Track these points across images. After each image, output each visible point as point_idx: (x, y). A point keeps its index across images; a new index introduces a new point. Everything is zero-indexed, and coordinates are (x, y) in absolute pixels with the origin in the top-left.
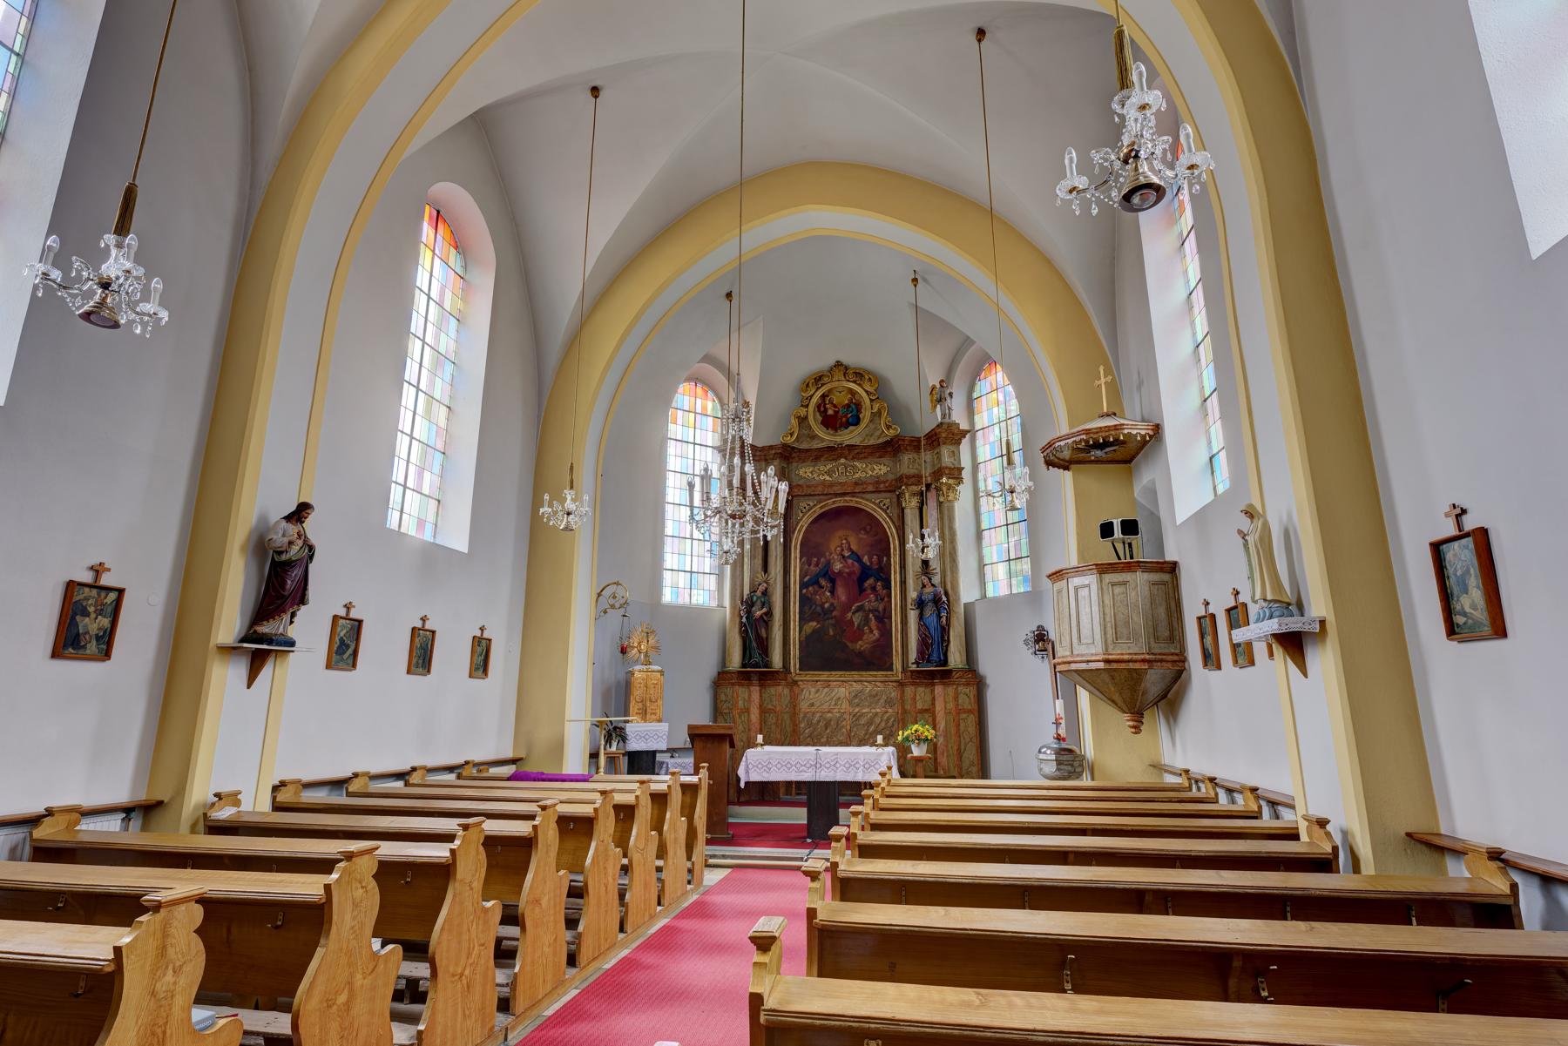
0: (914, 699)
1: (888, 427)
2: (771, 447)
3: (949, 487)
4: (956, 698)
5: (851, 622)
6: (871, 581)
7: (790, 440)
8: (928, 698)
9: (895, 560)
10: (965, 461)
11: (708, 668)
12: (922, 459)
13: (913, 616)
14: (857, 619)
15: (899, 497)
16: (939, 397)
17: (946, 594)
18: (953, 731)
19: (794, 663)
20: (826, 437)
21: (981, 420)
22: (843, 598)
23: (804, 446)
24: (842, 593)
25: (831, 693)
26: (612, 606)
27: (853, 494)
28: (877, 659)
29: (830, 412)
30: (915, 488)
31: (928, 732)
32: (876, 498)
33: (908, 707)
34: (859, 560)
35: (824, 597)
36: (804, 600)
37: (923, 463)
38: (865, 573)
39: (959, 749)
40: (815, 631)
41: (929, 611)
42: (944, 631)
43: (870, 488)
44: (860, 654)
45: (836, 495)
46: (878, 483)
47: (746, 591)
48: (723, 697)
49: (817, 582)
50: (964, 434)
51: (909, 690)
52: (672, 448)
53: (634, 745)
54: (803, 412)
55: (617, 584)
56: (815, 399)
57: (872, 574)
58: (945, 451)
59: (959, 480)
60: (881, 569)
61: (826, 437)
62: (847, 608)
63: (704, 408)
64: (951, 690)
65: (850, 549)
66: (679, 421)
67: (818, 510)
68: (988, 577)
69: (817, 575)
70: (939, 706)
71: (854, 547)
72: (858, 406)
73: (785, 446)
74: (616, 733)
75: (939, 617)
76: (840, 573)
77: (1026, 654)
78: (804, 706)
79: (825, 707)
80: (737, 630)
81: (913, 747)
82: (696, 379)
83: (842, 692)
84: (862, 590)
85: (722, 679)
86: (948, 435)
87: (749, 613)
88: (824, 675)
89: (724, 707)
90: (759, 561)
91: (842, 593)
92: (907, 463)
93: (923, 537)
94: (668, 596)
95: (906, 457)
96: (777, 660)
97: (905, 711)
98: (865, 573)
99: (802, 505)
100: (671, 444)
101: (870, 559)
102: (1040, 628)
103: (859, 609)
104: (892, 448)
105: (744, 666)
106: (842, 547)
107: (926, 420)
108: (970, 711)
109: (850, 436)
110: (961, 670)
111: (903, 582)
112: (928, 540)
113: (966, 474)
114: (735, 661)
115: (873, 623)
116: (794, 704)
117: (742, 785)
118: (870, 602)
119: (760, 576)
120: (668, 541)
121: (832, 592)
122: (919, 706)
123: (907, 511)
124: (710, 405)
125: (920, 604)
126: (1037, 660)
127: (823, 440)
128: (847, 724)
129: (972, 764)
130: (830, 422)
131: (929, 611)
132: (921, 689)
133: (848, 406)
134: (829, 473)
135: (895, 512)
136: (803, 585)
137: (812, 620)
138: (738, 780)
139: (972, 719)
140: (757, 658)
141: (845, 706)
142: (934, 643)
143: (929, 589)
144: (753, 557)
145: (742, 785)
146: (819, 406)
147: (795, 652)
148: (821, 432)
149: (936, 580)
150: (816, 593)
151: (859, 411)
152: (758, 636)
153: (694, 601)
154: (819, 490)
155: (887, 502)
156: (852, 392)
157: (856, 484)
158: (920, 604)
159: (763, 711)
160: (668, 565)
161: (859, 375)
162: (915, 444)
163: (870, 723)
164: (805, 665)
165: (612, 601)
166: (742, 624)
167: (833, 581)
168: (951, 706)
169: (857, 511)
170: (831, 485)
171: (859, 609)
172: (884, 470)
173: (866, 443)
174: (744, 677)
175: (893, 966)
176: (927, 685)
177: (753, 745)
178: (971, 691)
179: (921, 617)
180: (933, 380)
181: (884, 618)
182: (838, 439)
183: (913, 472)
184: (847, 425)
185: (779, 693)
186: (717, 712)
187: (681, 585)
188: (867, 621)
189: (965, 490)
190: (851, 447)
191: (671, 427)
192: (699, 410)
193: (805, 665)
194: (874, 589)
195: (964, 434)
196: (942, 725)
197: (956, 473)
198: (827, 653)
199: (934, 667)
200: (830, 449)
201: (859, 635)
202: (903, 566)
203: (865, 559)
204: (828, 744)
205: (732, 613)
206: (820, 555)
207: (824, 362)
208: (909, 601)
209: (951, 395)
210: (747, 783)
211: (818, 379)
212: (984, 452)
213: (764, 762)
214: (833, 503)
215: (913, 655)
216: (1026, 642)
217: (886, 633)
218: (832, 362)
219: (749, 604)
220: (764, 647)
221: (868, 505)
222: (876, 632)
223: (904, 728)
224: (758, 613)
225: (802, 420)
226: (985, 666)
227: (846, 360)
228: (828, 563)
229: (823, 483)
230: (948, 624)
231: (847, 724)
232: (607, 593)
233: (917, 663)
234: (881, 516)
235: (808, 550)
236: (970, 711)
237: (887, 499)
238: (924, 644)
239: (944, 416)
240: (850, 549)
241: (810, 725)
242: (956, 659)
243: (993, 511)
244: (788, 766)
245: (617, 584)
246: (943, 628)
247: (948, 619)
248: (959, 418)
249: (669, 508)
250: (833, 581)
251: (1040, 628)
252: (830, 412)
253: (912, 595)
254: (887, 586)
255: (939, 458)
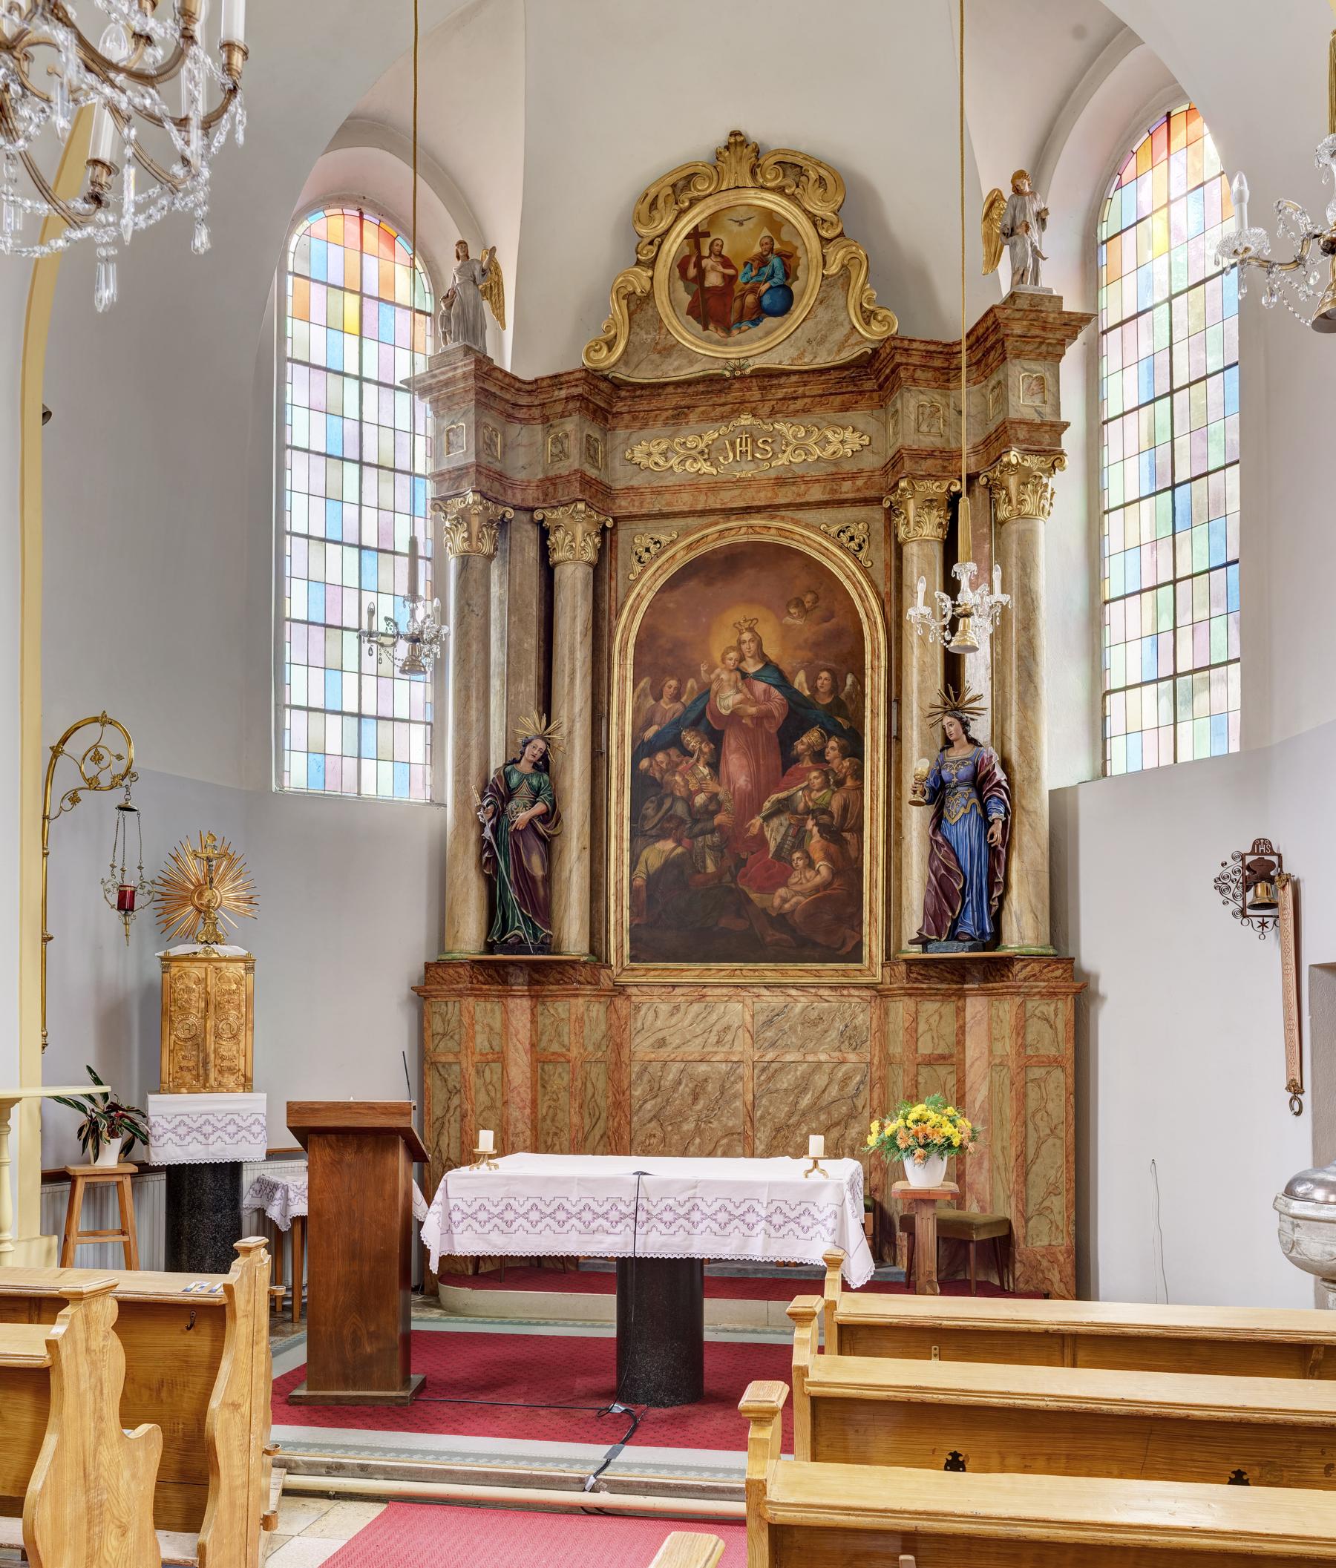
0: (913, 1032)
1: (868, 317)
2: (557, 380)
3: (1028, 478)
4: (1021, 1030)
5: (761, 840)
6: (812, 737)
7: (605, 360)
8: (949, 1028)
9: (875, 682)
10: (1072, 408)
11: (401, 943)
12: (963, 397)
13: (916, 820)
14: (775, 832)
15: (891, 513)
16: (1009, 223)
17: (1005, 764)
18: (1009, 1111)
19: (618, 941)
20: (702, 351)
21: (1114, 304)
22: (742, 781)
23: (644, 375)
24: (738, 769)
25: (705, 1018)
26: (93, 784)
27: (771, 509)
28: (826, 933)
29: (713, 280)
30: (935, 488)
31: (953, 1127)
32: (832, 519)
33: (896, 1049)
34: (783, 682)
35: (692, 781)
36: (644, 786)
37: (962, 414)
38: (800, 714)
39: (1022, 1155)
40: (669, 864)
41: (960, 806)
42: (996, 859)
43: (816, 494)
44: (781, 920)
45: (728, 512)
46: (836, 478)
47: (497, 761)
48: (437, 1025)
49: (677, 742)
50: (1074, 324)
51: (901, 1009)
52: (299, 388)
53: (167, 1151)
54: (640, 281)
55: (103, 720)
56: (674, 245)
57: (818, 721)
58: (1019, 375)
59: (1054, 458)
60: (838, 706)
61: (702, 351)
62: (750, 804)
63: (387, 282)
64: (1007, 1009)
65: (761, 656)
66: (318, 314)
67: (680, 556)
68: (1114, 725)
69: (678, 724)
70: (974, 1050)
71: (772, 651)
72: (789, 260)
73: (592, 377)
74: (115, 1120)
75: (986, 823)
76: (735, 716)
77: (1218, 914)
78: (641, 1047)
79: (694, 1049)
80: (472, 849)
81: (909, 1164)
82: (354, 198)
83: (736, 1011)
84: (788, 761)
85: (434, 982)
86: (1028, 332)
87: (499, 814)
88: (692, 972)
89: (444, 1052)
90: (529, 686)
91: (738, 769)
92: (915, 416)
93: (952, 587)
94: (297, 773)
95: (912, 402)
96: (572, 933)
97: (888, 1060)
98: (800, 714)
99: (642, 541)
100: (297, 375)
101: (812, 680)
102: (1262, 846)
103: (783, 807)
104: (869, 377)
105: (490, 947)
106: (741, 647)
107: (963, 294)
108: (1054, 1062)
109: (764, 347)
110: (1037, 958)
111: (894, 738)
112: (967, 596)
113: (1071, 442)
114: (469, 935)
115: (816, 842)
116: (616, 1044)
117: (434, 1266)
118: (809, 788)
119: (532, 722)
120: (295, 634)
121: (714, 766)
122: (925, 1047)
123: (912, 550)
124: (402, 276)
125: (937, 792)
126: (1247, 932)
127: (692, 358)
128: (745, 1089)
129: (1053, 1191)
130: (714, 309)
131: (960, 806)
132: (930, 1007)
133: (762, 261)
134: (707, 454)
135: (878, 556)
136: (642, 749)
137: (662, 836)
138: (424, 1253)
139: (1059, 1081)
140: (519, 931)
141: (742, 1047)
142: (967, 893)
143: (961, 752)
144: (512, 677)
145: (434, 1266)
146: (682, 265)
147: (619, 914)
148: (685, 333)
149: (981, 729)
150: (673, 767)
151: (789, 273)
152: (524, 876)
153: (368, 789)
154: (684, 501)
155: (859, 530)
156: (771, 219)
157: (780, 482)
158: (937, 792)
159: (541, 1060)
160: (296, 694)
161: (793, 170)
162: (941, 363)
163: (802, 1087)
164: (642, 950)
165: (90, 769)
166: (484, 845)
167: (716, 738)
168: (1006, 1047)
169: (780, 554)
170: (714, 488)
171: (783, 807)
172: (854, 441)
173: (808, 363)
174: (492, 972)
175: (845, 1449)
176: (946, 996)
177: (469, 1156)
178: (1062, 1010)
179: (938, 821)
180: (994, 176)
181: (842, 831)
182: (732, 352)
183: (928, 441)
184: (759, 313)
185: (577, 1015)
186: (426, 1061)
187: (333, 747)
188: (799, 839)
189: (1066, 486)
190: (767, 377)
191: (295, 328)
192: (371, 287)
193: (642, 950)
194: (818, 755)
195: (1074, 324)
196: (979, 1094)
197: (1045, 440)
198: (703, 918)
199: (967, 953)
200: (713, 384)
201: (779, 872)
202: (895, 699)
203: (800, 682)
204: (665, 1148)
205: (460, 819)
206: (685, 670)
207: (697, 139)
208: (909, 782)
209: (1041, 218)
210: (443, 1259)
211: (682, 186)
212: (1122, 389)
213: (491, 1202)
214: (716, 536)
215: (913, 921)
216: (1221, 885)
217: (848, 869)
218: (721, 138)
219: (499, 793)
220: (539, 902)
221: (812, 537)
222: (823, 868)
223: (884, 1112)
224: (523, 817)
225: (638, 303)
226: (1094, 950)
227: (755, 133)
228: (706, 693)
229: (695, 484)
230: (1008, 844)
231: (745, 1089)
232: (76, 747)
233: (923, 942)
234: (841, 566)
235: (656, 657)
236: (1054, 1062)
237: (861, 521)
238: (944, 891)
239: (1019, 275)
240: (761, 656)
241: (654, 1092)
242: (1022, 928)
243: (1134, 538)
244: (558, 1214)
245: (103, 720)
246: (993, 852)
247: (1007, 828)
248: (1058, 279)
249: (295, 548)
250: (716, 738)
251: (1262, 846)
252: (713, 280)
253: (918, 765)
254: (854, 749)
255: (1002, 400)
